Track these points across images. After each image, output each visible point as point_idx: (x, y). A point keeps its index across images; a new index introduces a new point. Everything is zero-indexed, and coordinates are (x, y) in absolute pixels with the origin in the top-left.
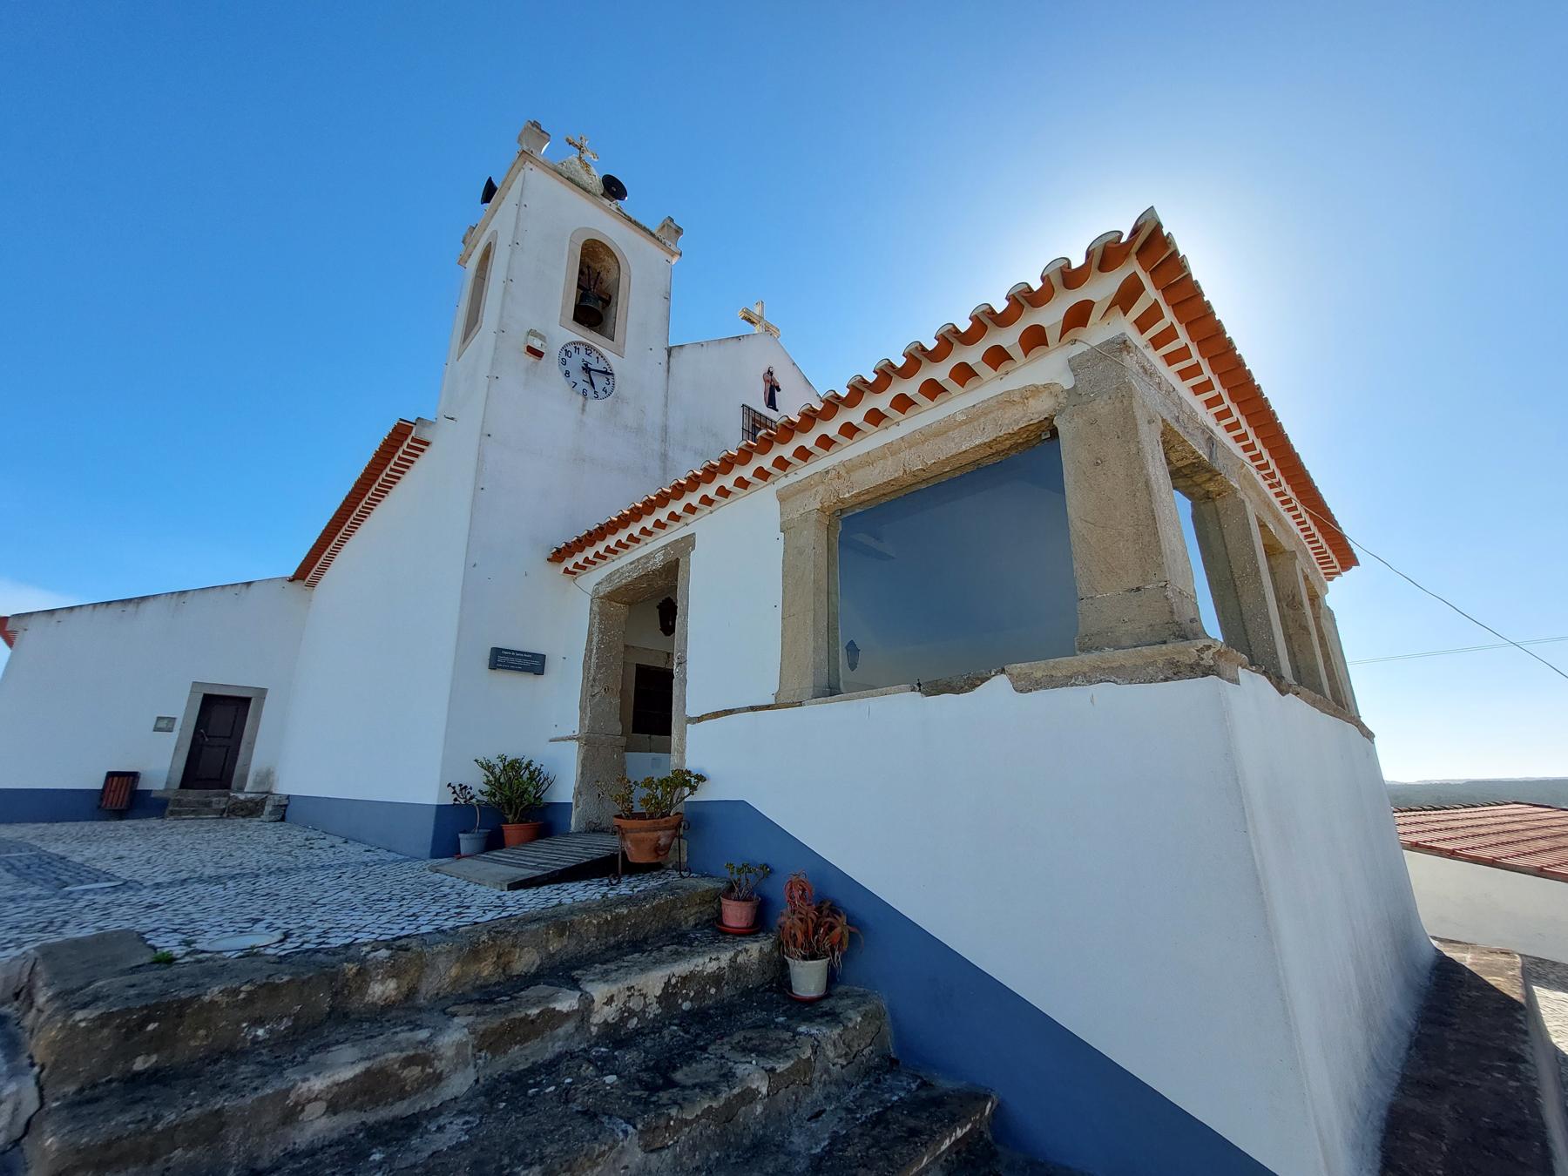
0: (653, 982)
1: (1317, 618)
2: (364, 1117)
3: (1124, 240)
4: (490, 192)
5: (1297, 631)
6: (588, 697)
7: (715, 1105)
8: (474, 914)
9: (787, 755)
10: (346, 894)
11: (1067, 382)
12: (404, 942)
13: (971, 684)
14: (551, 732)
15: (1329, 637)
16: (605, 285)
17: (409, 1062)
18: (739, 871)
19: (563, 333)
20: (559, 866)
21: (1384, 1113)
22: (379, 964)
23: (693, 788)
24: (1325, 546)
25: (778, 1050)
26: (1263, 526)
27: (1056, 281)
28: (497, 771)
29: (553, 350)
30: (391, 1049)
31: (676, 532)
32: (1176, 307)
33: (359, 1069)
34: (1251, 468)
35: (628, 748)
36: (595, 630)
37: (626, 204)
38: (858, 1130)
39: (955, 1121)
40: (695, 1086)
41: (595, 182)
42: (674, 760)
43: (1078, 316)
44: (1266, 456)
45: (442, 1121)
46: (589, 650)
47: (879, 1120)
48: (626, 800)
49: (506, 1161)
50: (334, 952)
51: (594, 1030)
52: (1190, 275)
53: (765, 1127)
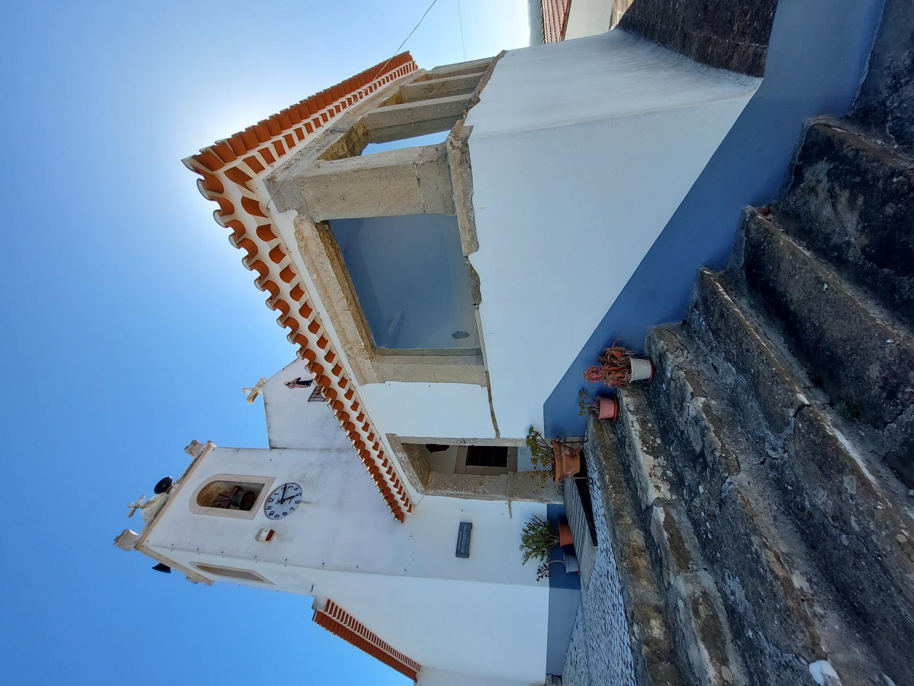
0: (646, 461)
1: (439, 76)
2: (729, 641)
3: (202, 178)
4: (162, 568)
5: (445, 89)
6: (485, 496)
7: (712, 429)
8: (612, 569)
9: (516, 384)
10: (602, 646)
11: (293, 214)
12: (629, 615)
13: (474, 276)
14: (504, 516)
15: (452, 70)
16: (228, 490)
17: (696, 613)
18: (583, 408)
19: (258, 517)
20: (583, 515)
21: (699, 65)
22: (642, 631)
23: (537, 434)
24: (398, 69)
25: (681, 390)
26: (384, 104)
27: (229, 218)
28: (529, 550)
29: (269, 523)
30: (691, 626)
31: (385, 445)
32: (248, 148)
33: (702, 646)
34: (349, 108)
35: (515, 470)
36: (445, 492)
37: (174, 478)
38: (722, 346)
39: (715, 292)
40: (703, 440)
41: (162, 496)
42: (522, 445)
43: (252, 206)
44: (343, 99)
45: (728, 592)
46: (457, 496)
47: (715, 332)
48: (544, 474)
49: (749, 556)
50: (636, 659)
51: (674, 497)
52: (228, 140)
53: (723, 399)
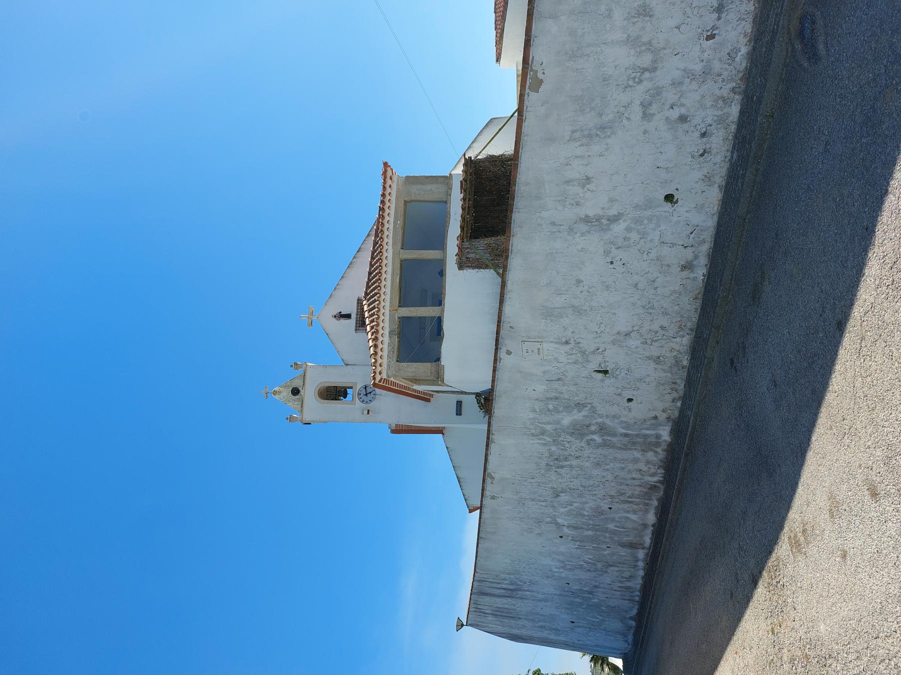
37: (297, 383)
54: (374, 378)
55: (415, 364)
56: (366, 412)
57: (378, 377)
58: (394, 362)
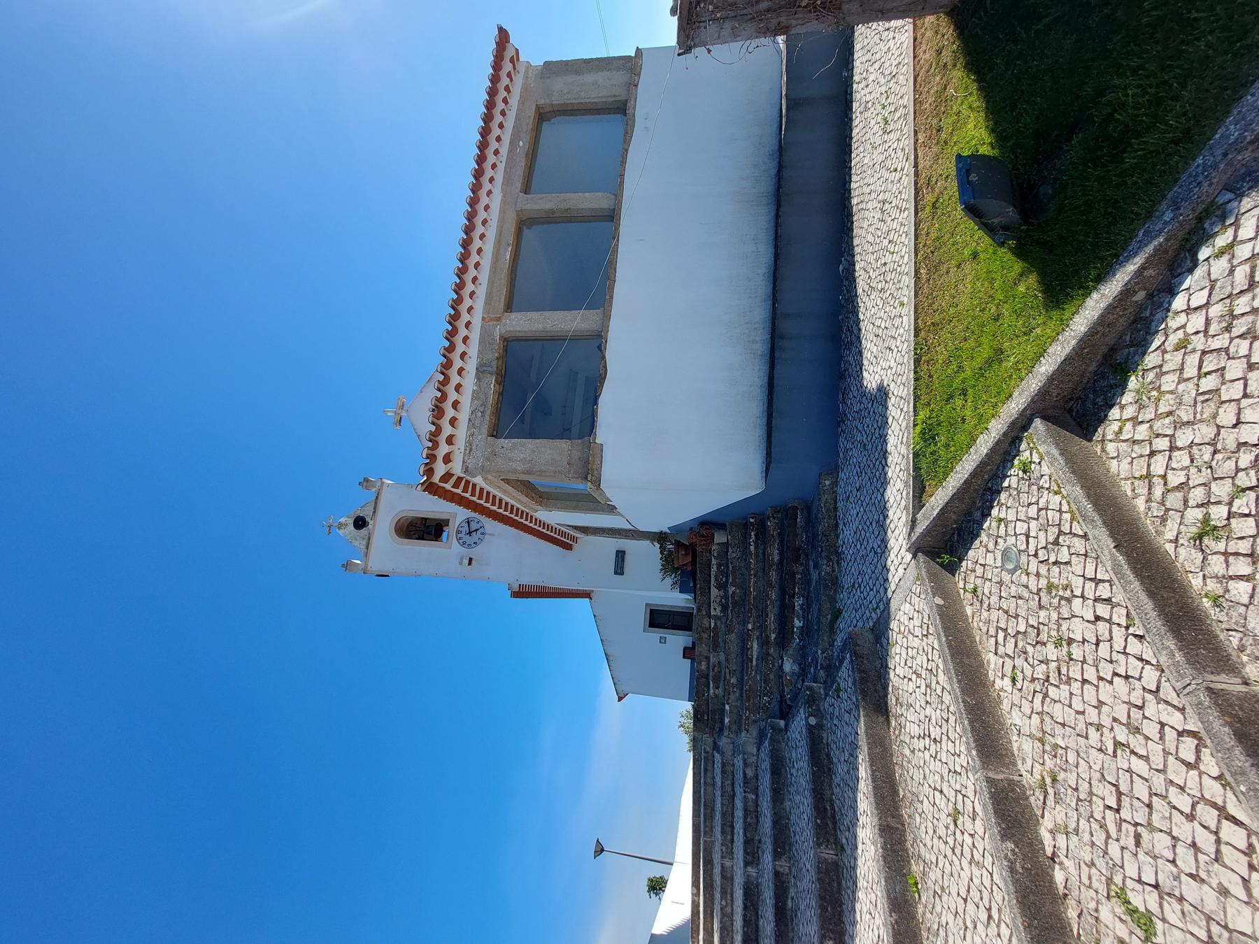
13: (548, 64)
37: (367, 513)
54: (430, 472)
55: (531, 444)
56: (466, 562)
57: (440, 469)
58: (482, 436)
